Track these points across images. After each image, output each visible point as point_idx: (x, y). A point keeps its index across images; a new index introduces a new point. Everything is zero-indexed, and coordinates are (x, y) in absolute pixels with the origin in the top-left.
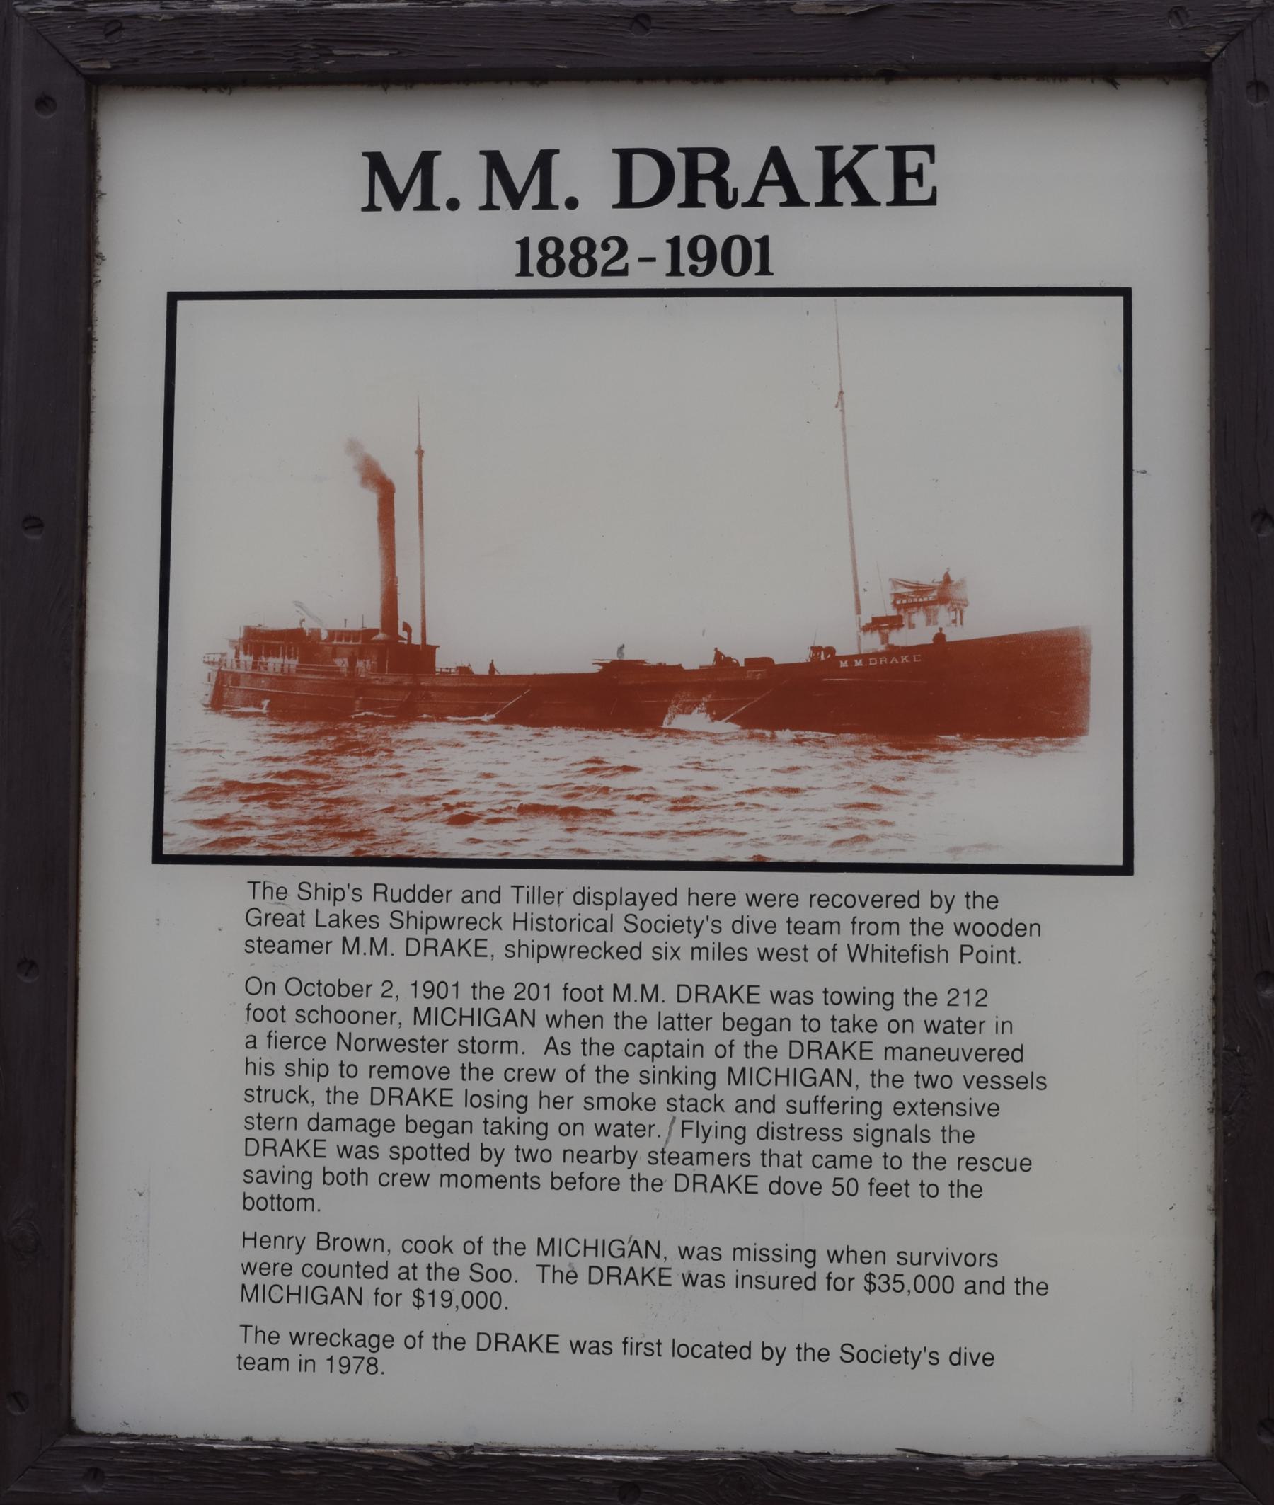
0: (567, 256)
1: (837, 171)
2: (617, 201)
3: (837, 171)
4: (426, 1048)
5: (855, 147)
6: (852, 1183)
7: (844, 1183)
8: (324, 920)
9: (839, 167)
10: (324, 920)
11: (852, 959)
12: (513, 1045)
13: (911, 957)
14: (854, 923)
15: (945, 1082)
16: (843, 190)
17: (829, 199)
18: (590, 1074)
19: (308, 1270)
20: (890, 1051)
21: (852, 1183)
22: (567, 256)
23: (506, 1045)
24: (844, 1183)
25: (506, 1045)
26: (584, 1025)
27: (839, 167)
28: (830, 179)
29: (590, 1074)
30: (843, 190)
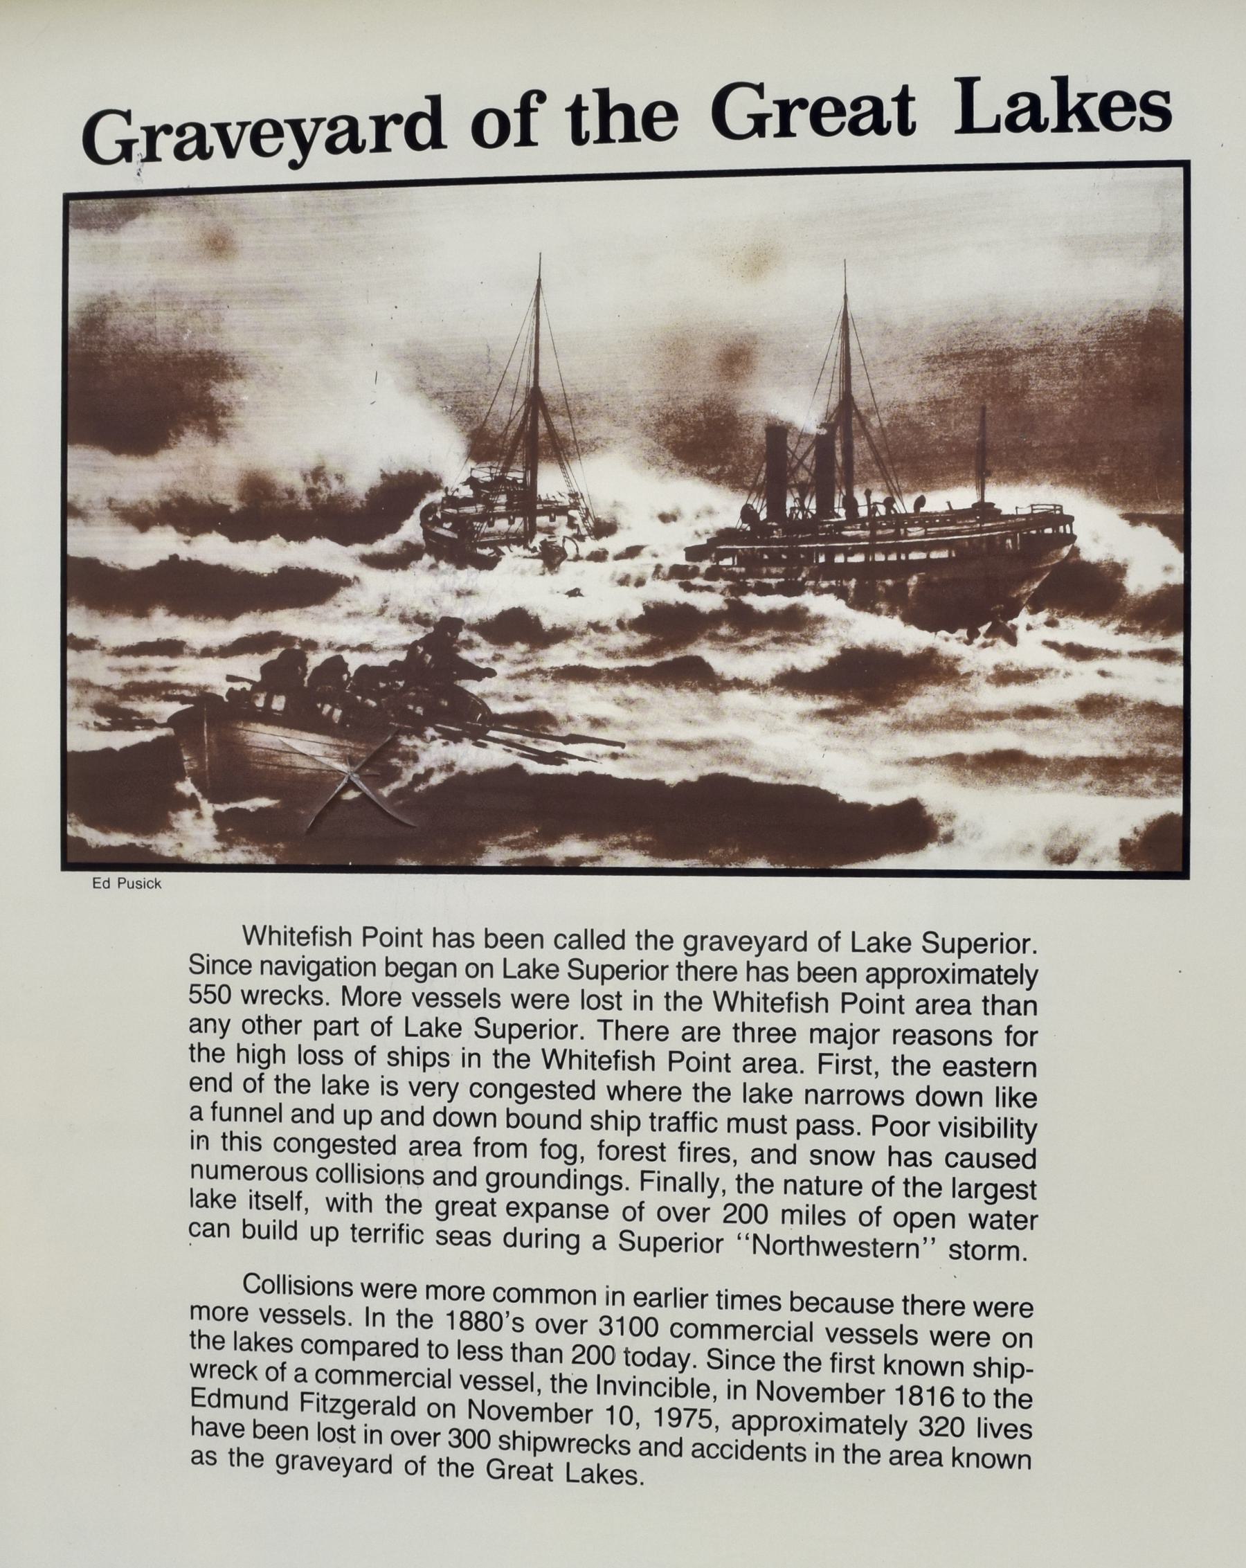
0: (474, 1320)
1: (1070, 108)
2: (959, 126)
3: (1070, 108)
4: (565, 1095)
5: (1079, 95)
6: (225, 990)
7: (215, 990)
8: (576, 1474)
9: (1071, 106)
10: (576, 1474)
11: (720, 1008)
12: (1013, 1251)
13: (613, 1064)
14: (477, 1143)
15: (255, 1144)
16: (1074, 122)
17: (1063, 127)
18: (898, 1187)
19: (500, 1295)
20: (816, 1033)
21: (225, 990)
22: (474, 1320)
23: (1004, 1251)
24: (215, 990)
25: (1004, 1251)
26: (270, 1118)
27: (1071, 106)
28: (1063, 114)
29: (898, 1187)
30: (1074, 122)
